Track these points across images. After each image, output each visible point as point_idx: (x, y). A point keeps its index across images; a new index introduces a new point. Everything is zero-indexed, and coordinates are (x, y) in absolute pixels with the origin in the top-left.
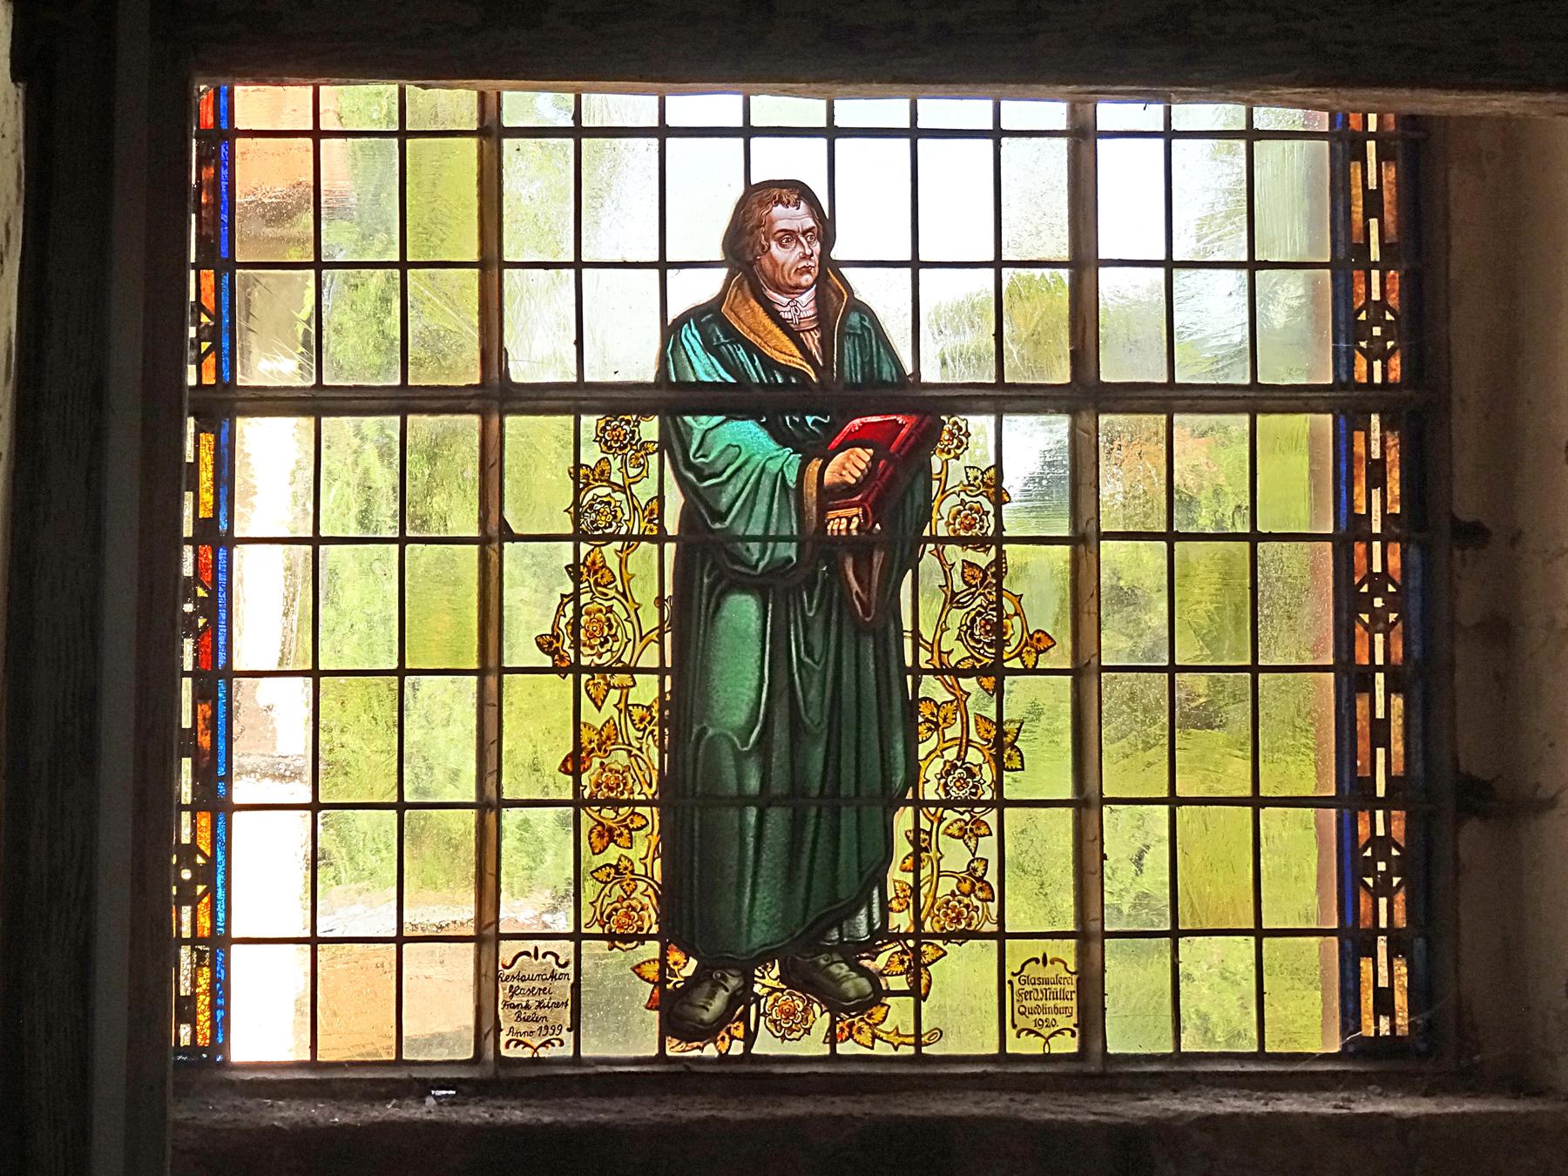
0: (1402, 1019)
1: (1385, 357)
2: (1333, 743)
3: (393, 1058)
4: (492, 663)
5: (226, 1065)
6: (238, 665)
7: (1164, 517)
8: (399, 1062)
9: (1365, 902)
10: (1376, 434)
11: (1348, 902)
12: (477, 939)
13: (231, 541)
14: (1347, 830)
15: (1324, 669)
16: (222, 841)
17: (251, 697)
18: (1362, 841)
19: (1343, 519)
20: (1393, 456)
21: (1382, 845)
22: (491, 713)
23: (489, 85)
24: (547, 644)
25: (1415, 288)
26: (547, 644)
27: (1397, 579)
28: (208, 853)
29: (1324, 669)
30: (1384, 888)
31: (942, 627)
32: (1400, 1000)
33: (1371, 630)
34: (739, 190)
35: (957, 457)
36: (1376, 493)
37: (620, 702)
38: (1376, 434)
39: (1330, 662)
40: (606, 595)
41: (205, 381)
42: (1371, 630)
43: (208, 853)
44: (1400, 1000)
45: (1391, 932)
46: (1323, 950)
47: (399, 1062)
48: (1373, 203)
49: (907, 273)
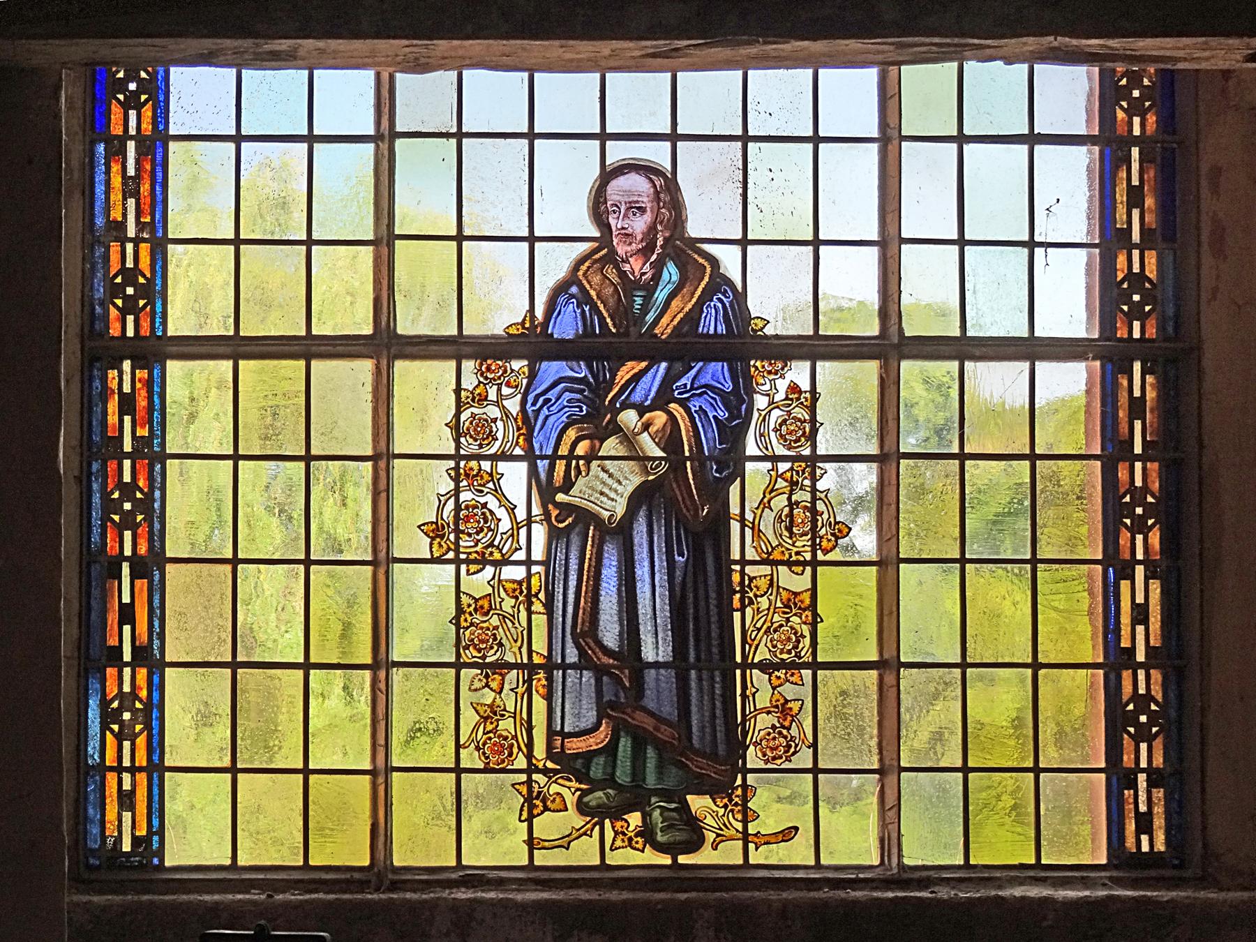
0: (1160, 838)
1: (1143, 318)
2: (1099, 488)
3: (301, 863)
4: (382, 555)
5: (161, 867)
6: (168, 762)
7: (960, 755)
8: (306, 866)
9: (1125, 537)
10: (1135, 166)
11: (1107, 117)
12: (374, 667)
13: (163, 457)
14: (1112, 691)
15: (1095, 457)
16: (158, 483)
17: (179, 791)
18: (1125, 698)
19: (1111, 651)
20: (1159, 810)
21: (1143, 701)
22: (382, 697)
23: (379, 69)
24: (435, 531)
25: (1173, 470)
26: (435, 531)
27: (1159, 697)
28: (148, 275)
29: (1095, 457)
30: (1140, 527)
31: (765, 505)
32: (1159, 822)
33: (1137, 740)
34: (596, 172)
35: (782, 377)
36: (1137, 393)
37: (493, 578)
38: (1135, 166)
39: (1100, 557)
40: (482, 491)
41: (142, 333)
42: (1137, 740)
43: (148, 275)
44: (1159, 822)
45: (1149, 771)
46: (1090, 257)
47: (306, 866)
48: (1137, 407)
49: (739, 131)
